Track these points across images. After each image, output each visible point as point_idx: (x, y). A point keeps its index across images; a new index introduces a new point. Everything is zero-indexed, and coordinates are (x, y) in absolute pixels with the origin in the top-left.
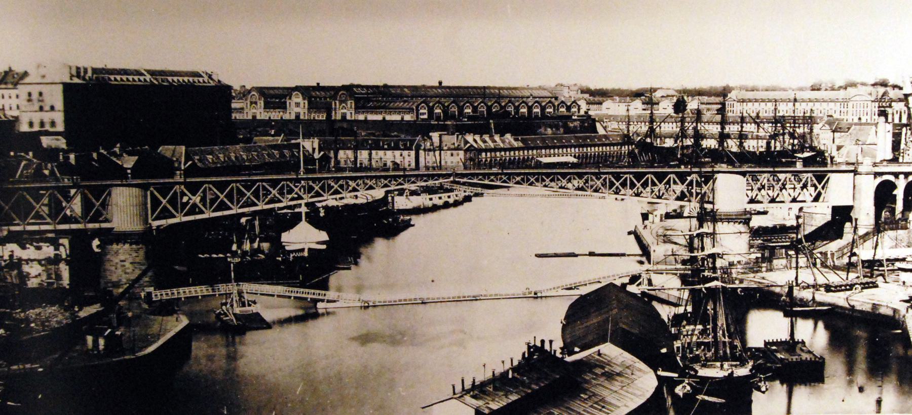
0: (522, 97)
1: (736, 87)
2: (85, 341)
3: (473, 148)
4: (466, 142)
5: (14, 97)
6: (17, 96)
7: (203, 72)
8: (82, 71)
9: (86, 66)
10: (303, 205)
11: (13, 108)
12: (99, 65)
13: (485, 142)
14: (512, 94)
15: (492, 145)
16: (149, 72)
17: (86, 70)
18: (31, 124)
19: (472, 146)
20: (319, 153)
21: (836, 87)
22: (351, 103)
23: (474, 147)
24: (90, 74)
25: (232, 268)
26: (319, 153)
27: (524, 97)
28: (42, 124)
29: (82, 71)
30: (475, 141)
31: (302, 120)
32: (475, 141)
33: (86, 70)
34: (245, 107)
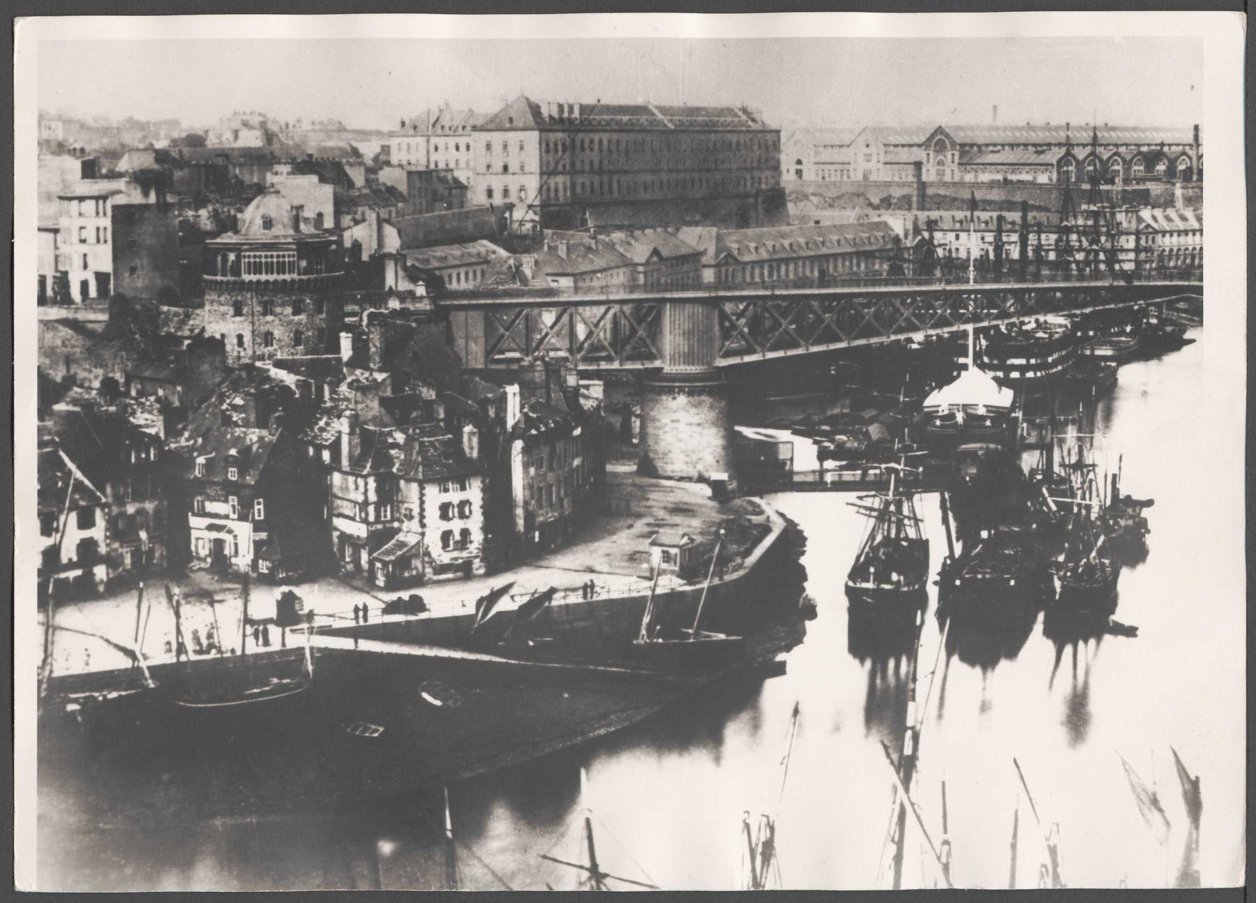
0: (1116, 145)
1: (38, 675)
2: (73, 712)
3: (1150, 230)
4: (1140, 220)
5: (463, 148)
6: (468, 148)
7: (740, 109)
8: (566, 109)
9: (571, 101)
10: (86, 534)
11: (511, 170)
12: (589, 100)
13: (1168, 219)
14: (1119, 138)
15: (1181, 225)
16: (659, 108)
17: (571, 108)
18: (490, 193)
19: (1148, 226)
20: (914, 238)
21: (1022, 147)
22: (953, 155)
23: (1153, 228)
24: (576, 114)
25: (1107, 307)
26: (914, 238)
27: (1131, 145)
28: (506, 192)
29: (566, 109)
30: (1154, 218)
31: (481, 210)
32: (1154, 218)
33: (571, 108)
34: (924, 161)
